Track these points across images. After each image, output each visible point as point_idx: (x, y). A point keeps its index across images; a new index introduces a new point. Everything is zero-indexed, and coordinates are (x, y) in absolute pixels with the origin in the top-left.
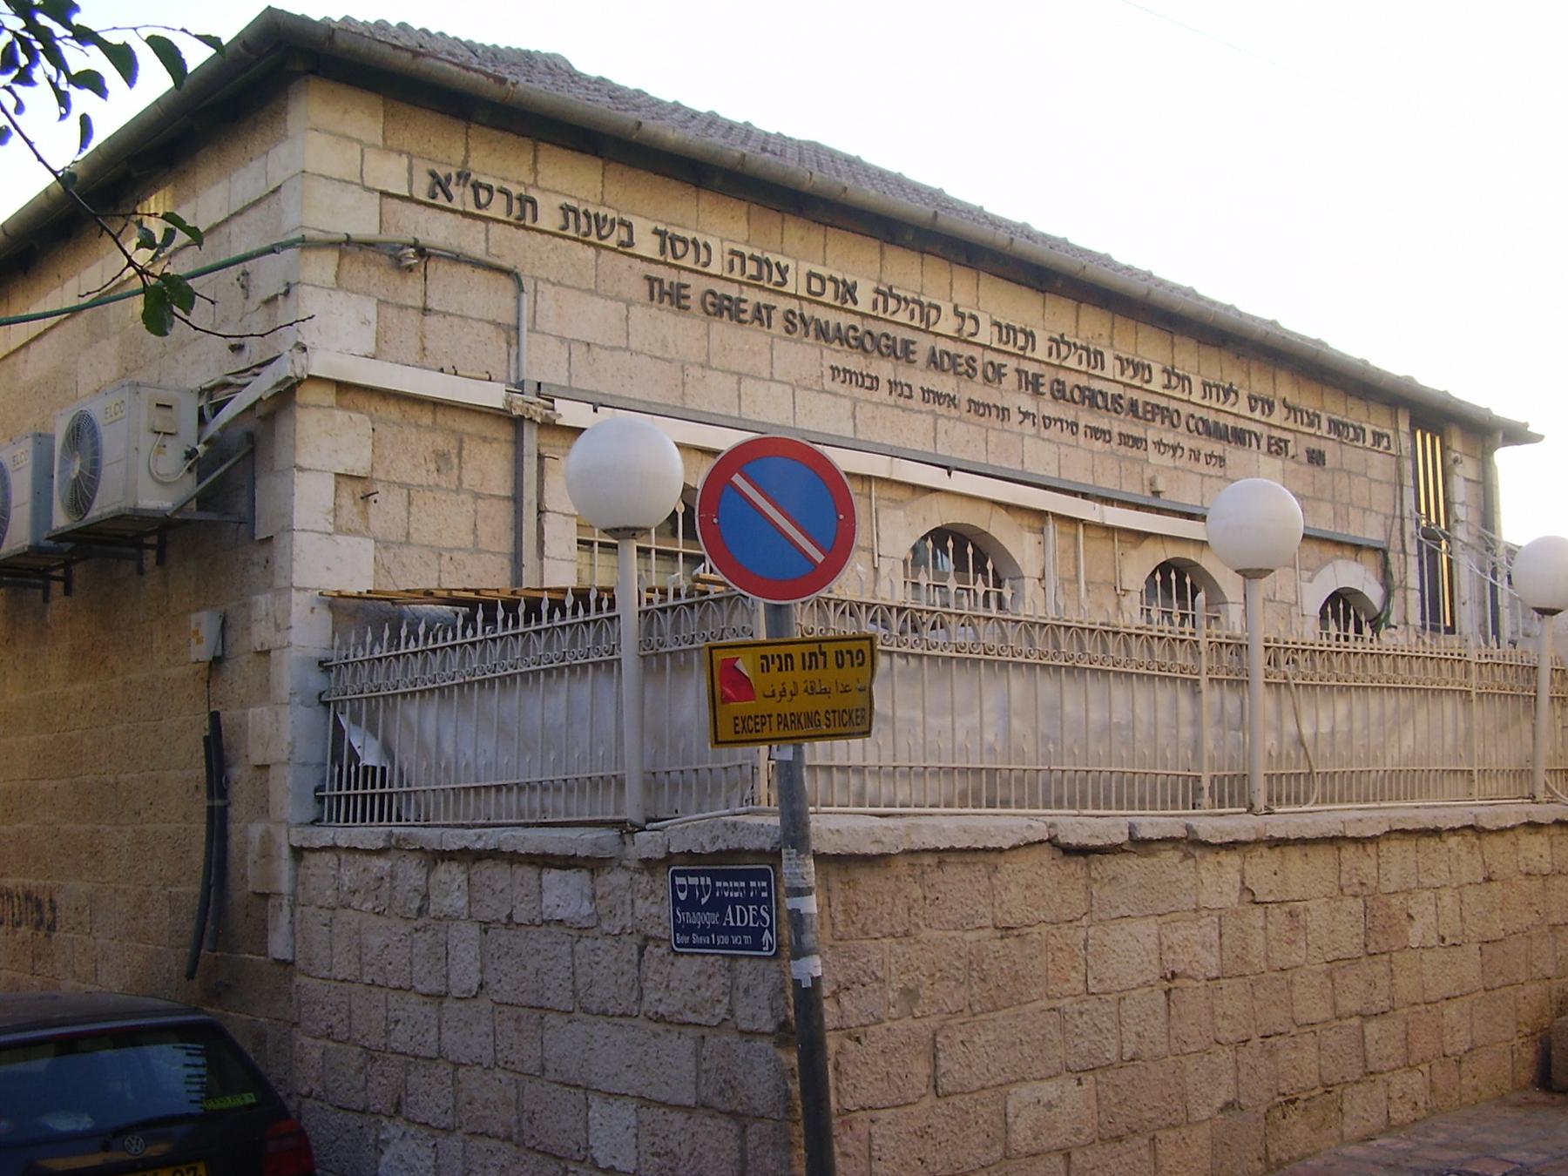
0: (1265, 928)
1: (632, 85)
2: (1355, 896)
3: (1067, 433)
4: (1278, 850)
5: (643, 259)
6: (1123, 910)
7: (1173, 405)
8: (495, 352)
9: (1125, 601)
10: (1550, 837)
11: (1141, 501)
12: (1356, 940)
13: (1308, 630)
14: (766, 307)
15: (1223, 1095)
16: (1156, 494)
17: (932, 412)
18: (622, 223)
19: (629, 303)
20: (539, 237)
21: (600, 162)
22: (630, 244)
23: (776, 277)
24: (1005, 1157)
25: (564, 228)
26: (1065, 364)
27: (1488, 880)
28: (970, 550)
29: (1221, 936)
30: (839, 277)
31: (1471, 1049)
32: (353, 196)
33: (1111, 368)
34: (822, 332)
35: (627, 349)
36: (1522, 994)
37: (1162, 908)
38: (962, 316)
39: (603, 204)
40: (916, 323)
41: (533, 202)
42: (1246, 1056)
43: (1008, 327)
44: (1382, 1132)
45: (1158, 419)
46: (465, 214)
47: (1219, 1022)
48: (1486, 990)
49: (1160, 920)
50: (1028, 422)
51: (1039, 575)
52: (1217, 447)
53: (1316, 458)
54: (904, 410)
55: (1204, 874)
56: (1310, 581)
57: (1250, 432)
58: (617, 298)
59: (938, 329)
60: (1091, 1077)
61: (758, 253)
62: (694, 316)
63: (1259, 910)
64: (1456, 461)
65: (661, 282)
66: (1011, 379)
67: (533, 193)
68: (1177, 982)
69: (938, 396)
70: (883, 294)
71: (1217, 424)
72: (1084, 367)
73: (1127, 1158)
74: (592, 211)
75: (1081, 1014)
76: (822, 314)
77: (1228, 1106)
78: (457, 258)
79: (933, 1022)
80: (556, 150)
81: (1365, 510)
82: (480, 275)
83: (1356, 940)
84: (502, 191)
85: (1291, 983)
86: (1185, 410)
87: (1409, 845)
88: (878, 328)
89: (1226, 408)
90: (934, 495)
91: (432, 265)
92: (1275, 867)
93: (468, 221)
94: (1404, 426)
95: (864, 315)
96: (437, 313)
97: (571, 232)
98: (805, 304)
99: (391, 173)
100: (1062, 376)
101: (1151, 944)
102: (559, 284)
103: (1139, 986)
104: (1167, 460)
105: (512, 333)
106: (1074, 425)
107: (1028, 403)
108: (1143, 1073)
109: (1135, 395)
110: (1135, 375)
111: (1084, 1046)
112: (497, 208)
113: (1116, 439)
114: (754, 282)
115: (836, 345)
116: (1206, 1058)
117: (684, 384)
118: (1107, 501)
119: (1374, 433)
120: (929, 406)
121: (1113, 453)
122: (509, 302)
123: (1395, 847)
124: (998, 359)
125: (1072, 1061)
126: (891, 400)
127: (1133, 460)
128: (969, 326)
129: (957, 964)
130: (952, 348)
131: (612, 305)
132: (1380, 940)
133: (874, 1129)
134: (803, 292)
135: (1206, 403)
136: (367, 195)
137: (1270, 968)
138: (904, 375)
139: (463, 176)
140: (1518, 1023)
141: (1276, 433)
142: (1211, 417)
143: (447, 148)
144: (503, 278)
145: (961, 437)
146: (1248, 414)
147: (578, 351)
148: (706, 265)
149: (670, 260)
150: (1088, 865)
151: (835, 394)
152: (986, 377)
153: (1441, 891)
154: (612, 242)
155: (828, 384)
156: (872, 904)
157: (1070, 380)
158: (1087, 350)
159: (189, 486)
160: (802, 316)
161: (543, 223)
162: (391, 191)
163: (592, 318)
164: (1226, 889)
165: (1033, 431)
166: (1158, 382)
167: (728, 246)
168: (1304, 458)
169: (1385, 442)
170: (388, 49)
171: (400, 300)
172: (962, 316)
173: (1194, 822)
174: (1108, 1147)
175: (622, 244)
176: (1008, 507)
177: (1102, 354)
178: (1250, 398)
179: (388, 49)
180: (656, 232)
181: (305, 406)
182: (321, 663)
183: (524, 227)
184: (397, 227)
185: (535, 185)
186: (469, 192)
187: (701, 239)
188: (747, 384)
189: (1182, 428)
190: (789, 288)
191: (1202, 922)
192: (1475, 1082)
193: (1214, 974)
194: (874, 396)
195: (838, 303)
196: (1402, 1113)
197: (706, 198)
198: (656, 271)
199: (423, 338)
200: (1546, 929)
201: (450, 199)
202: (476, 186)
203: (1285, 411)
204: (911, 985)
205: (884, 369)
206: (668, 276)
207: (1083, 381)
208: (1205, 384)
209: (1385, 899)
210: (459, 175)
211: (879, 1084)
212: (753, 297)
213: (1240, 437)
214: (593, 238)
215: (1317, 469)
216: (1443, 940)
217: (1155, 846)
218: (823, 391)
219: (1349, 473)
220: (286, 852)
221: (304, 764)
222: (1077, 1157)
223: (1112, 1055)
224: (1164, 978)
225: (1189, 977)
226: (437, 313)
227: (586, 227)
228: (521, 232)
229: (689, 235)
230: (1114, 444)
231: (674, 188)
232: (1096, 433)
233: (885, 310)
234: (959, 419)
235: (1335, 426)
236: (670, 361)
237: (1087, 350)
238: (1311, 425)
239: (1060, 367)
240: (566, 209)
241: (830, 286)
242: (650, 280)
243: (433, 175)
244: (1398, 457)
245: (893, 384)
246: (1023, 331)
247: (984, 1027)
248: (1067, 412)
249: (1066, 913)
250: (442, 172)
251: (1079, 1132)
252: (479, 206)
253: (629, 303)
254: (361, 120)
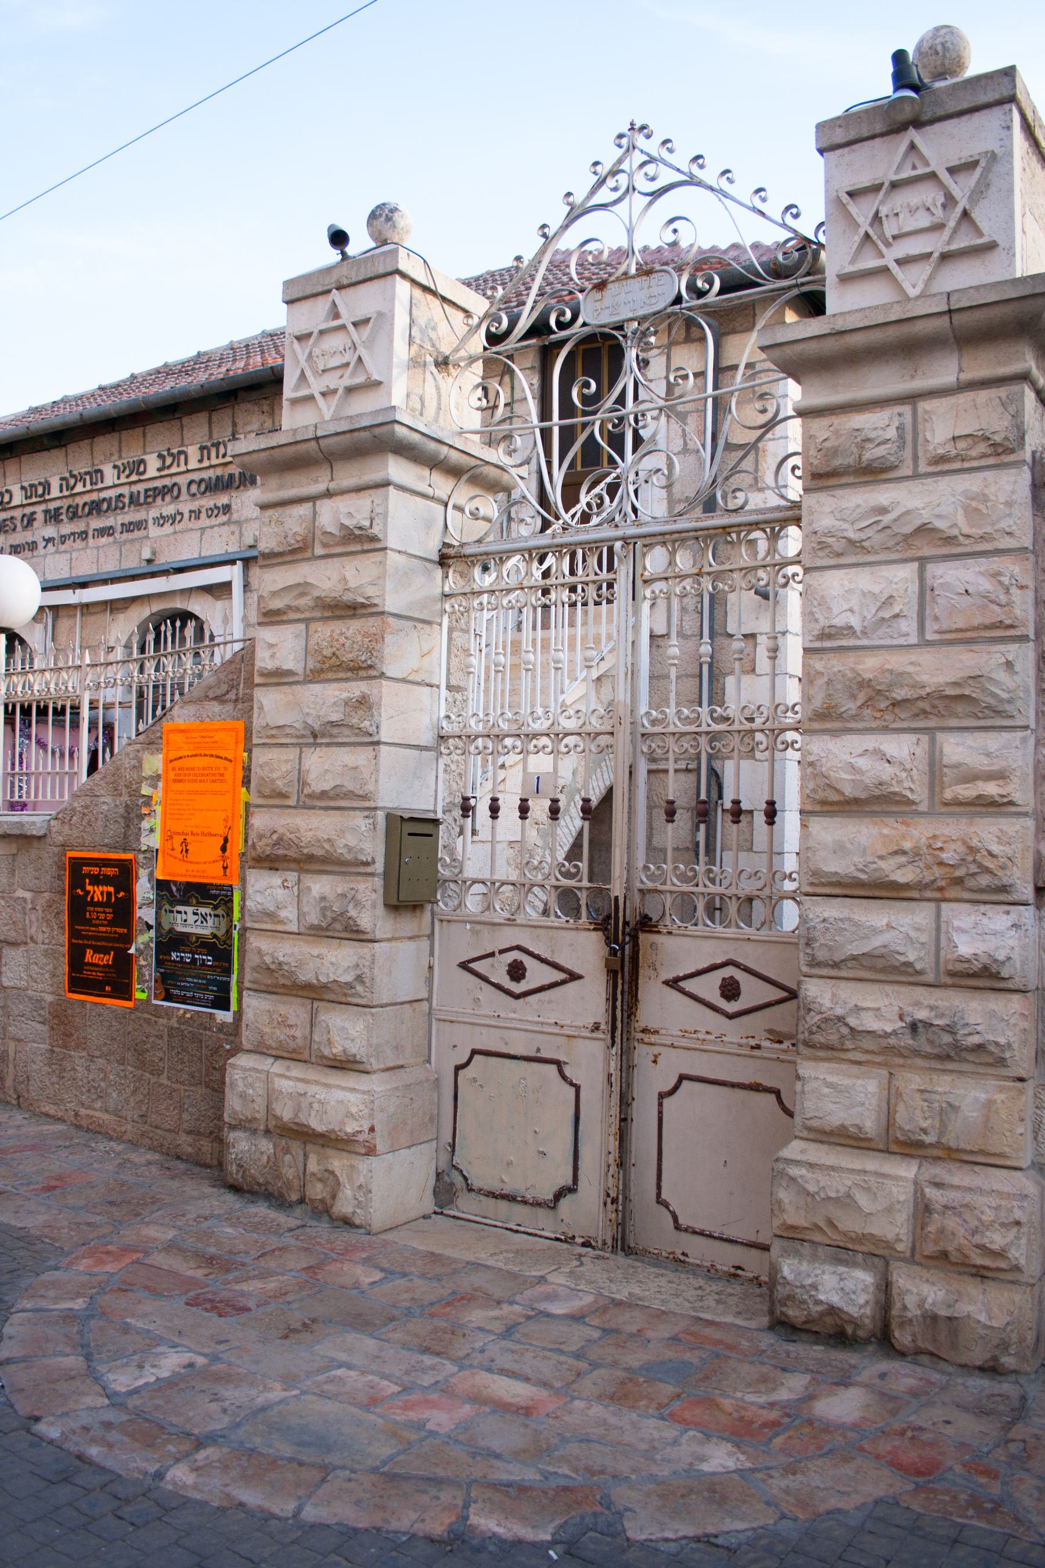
11: (139, 572)
33: (110, 476)
50: (50, 545)
52: (223, 499)
72: (88, 487)
86: (183, 480)
104: (168, 529)
109: (135, 488)
118: (84, 585)
189: (184, 495)
232: (103, 532)
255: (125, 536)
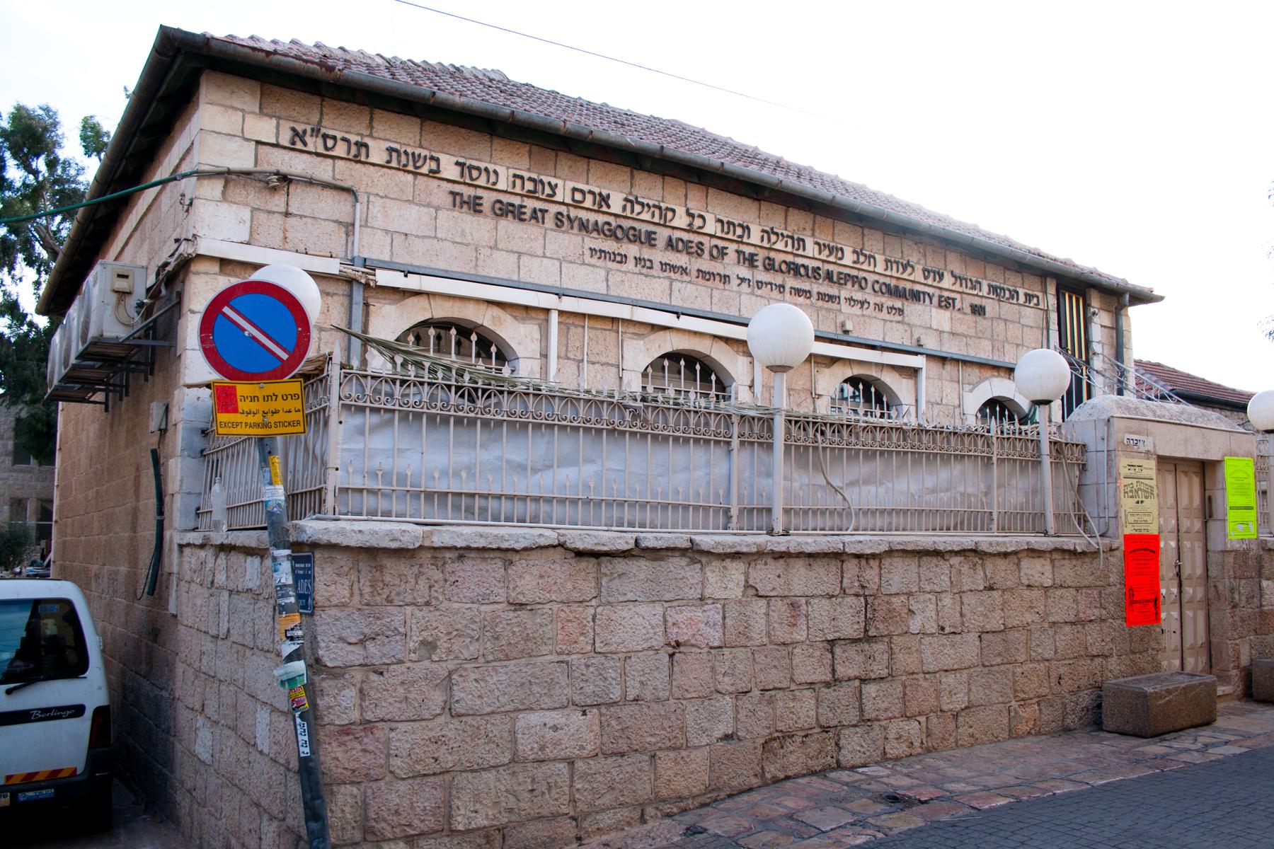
0: (767, 614)
1: (548, 87)
2: (857, 595)
3: (775, 292)
4: (781, 561)
5: (449, 181)
6: (630, 596)
7: (862, 274)
8: (337, 240)
9: (818, 402)
10: (1052, 561)
12: (856, 626)
13: (972, 422)
14: (541, 210)
15: (722, 729)
16: (846, 332)
17: (669, 278)
18: (432, 158)
19: (437, 209)
20: (372, 168)
21: (419, 121)
22: (438, 171)
23: (548, 190)
24: (513, 761)
25: (388, 162)
26: (775, 247)
27: (991, 588)
28: (698, 367)
29: (724, 618)
30: (597, 190)
31: (966, 708)
32: (236, 144)
33: (811, 249)
34: (584, 226)
35: (435, 237)
36: (1019, 670)
37: (668, 596)
38: (692, 216)
39: (421, 147)
40: (656, 220)
41: (366, 146)
42: (745, 702)
43: (729, 223)
44: (877, 763)
45: (849, 284)
46: (318, 155)
47: (720, 677)
48: (984, 666)
49: (666, 605)
50: (745, 285)
51: (749, 383)
52: (898, 304)
53: (978, 310)
54: (646, 276)
55: (709, 574)
56: (971, 391)
57: (924, 293)
58: (429, 205)
59: (674, 224)
60: (595, 710)
61: (534, 176)
62: (486, 216)
63: (763, 602)
64: (1094, 314)
65: (462, 195)
66: (732, 255)
67: (366, 140)
68: (682, 649)
69: (673, 268)
70: (631, 201)
71: (897, 287)
72: (789, 249)
73: (629, 769)
74: (410, 151)
75: (587, 666)
76: (583, 215)
77: (727, 737)
78: (311, 182)
79: (451, 665)
80: (386, 114)
81: (1018, 345)
82: (327, 193)
83: (856, 626)
84: (344, 139)
85: (791, 654)
86: (871, 278)
87: (912, 564)
88: (626, 224)
89: (905, 276)
90: (661, 333)
91: (292, 187)
92: (778, 572)
93: (319, 159)
94: (1052, 290)
95: (616, 216)
96: (296, 215)
97: (394, 164)
98: (571, 209)
99: (265, 129)
100: (772, 255)
101: (658, 620)
102: (386, 197)
103: (644, 650)
104: (856, 310)
105: (349, 227)
106: (781, 288)
107: (744, 272)
108: (645, 710)
109: (831, 267)
110: (831, 254)
111: (589, 689)
112: (340, 150)
113: (815, 296)
114: (531, 195)
115: (595, 234)
116: (707, 702)
117: (477, 259)
119: (1026, 295)
120: (665, 274)
121: (812, 305)
122: (348, 207)
123: (898, 565)
124: (721, 244)
125: (577, 698)
126: (637, 270)
127: (828, 310)
128: (698, 222)
129: (473, 626)
130: (685, 236)
131: (426, 210)
132: (881, 626)
133: (393, 734)
134: (569, 200)
135: (888, 273)
136: (246, 143)
137: (771, 642)
138: (647, 253)
139: (316, 131)
140: (1016, 691)
141: (946, 294)
142: (893, 283)
143: (305, 115)
144: (345, 195)
145: (690, 294)
146: (922, 280)
147: (398, 239)
148: (494, 184)
149: (468, 181)
150: (599, 564)
151: (593, 266)
152: (711, 255)
153: (943, 595)
154: (425, 170)
155: (587, 259)
156: (397, 582)
157: (779, 258)
158: (792, 238)
159: (138, 321)
160: (568, 216)
161: (374, 158)
162: (263, 140)
163: (411, 218)
164: (731, 585)
165: (749, 290)
166: (849, 259)
167: (512, 172)
168: (968, 310)
169: (1035, 300)
170: (249, 51)
171: (269, 208)
172: (692, 216)
173: (697, 538)
174: (610, 760)
175: (431, 171)
176: (727, 340)
177: (803, 240)
178: (924, 270)
179: (249, 51)
180: (457, 163)
181: (197, 273)
182: (203, 432)
183: (360, 162)
184: (268, 163)
185: (371, 136)
186: (320, 141)
187: (491, 167)
188: (525, 259)
189: (869, 289)
190: (558, 198)
191: (706, 607)
192: (971, 730)
193: (716, 644)
194: (624, 267)
195: (596, 208)
196: (894, 749)
197: (498, 143)
198: (457, 188)
199: (285, 231)
200: (1046, 625)
201: (305, 144)
202: (325, 137)
203: (953, 280)
204: (430, 639)
205: (632, 250)
206: (467, 192)
207: (790, 258)
208: (887, 261)
209: (886, 599)
210: (313, 130)
211: (398, 705)
212: (531, 204)
213: (916, 296)
214: (410, 168)
215: (979, 318)
216: (943, 629)
217: (664, 553)
218: (584, 264)
219: (1006, 320)
220: (176, 547)
221: (189, 493)
222: (580, 765)
223: (616, 694)
224: (669, 645)
225: (693, 645)
226: (296, 215)
227: (401, 162)
228: (359, 165)
229: (482, 165)
230: (814, 299)
231: (474, 136)
232: (799, 292)
233: (632, 211)
234: (690, 282)
235: (994, 289)
236: (467, 245)
237: (792, 238)
238: (973, 288)
239: (771, 249)
240: (391, 150)
241: (589, 198)
242: (453, 194)
243: (293, 130)
244: (1046, 311)
245: (638, 260)
246: (740, 225)
247: (496, 672)
248: (778, 279)
249: (576, 596)
250: (300, 128)
251: (582, 748)
252: (326, 148)
253: (437, 209)
254: (247, 99)
255: (820, 303)
